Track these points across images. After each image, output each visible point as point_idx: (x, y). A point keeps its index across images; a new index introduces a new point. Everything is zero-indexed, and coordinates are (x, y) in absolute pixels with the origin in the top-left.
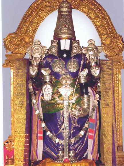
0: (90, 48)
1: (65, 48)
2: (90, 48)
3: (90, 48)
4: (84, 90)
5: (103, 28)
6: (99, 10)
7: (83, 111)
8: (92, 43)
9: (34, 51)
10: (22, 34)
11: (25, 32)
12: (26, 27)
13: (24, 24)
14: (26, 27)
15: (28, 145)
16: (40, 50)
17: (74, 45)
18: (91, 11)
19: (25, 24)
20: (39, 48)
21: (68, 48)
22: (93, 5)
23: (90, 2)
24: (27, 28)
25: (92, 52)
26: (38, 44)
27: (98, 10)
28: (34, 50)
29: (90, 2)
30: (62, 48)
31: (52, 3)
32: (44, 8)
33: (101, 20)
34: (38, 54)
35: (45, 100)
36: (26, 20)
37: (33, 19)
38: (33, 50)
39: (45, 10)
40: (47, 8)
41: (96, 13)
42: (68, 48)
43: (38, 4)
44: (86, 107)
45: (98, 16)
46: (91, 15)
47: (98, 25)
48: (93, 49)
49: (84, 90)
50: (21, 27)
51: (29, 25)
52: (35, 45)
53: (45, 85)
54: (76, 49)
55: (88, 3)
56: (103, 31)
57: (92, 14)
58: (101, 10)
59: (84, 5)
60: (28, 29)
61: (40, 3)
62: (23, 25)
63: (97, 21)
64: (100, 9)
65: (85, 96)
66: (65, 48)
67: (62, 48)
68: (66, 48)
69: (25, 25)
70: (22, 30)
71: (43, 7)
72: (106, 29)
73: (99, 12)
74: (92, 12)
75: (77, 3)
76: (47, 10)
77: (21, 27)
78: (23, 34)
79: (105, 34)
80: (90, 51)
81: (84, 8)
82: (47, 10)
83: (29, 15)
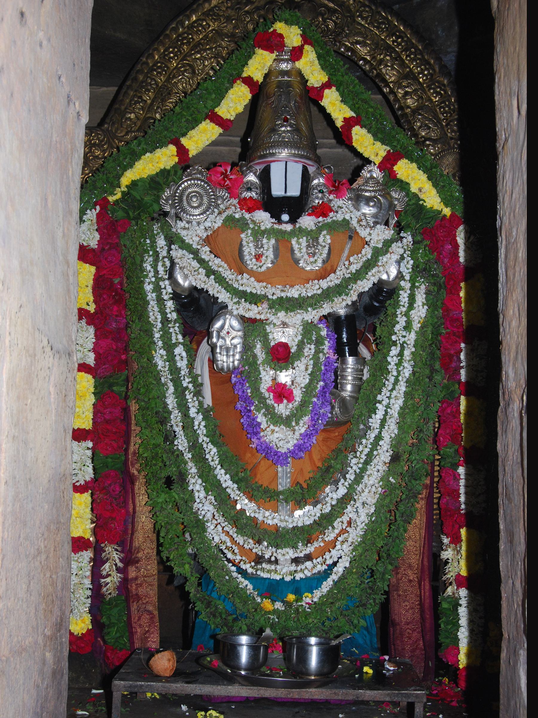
0: (367, 194)
1: (286, 192)
2: (367, 194)
3: (367, 191)
4: (344, 336)
5: (430, 120)
6: (415, 54)
7: (340, 408)
8: (375, 175)
9: (185, 203)
10: (127, 134)
11: (139, 123)
12: (143, 108)
13: (134, 96)
14: (143, 108)
15: (102, 691)
16: (205, 200)
17: (316, 182)
18: (385, 57)
19: (140, 97)
20: (201, 192)
21: (295, 191)
22: (390, 35)
23: (380, 23)
24: (148, 111)
25: (372, 206)
26: (198, 179)
27: (411, 53)
28: (185, 198)
29: (380, 23)
30: (277, 190)
31: (242, 21)
32: (213, 40)
33: (423, 89)
34: (197, 212)
35: (220, 366)
36: (142, 82)
37: (168, 80)
38: (181, 197)
39: (216, 48)
40: (223, 40)
41: (402, 64)
42: (295, 191)
43: (191, 26)
44: (349, 394)
45: (411, 76)
46: (384, 71)
47: (408, 107)
48: (375, 197)
49: (344, 336)
50: (126, 109)
51: (153, 101)
52: (190, 180)
53: (220, 317)
54: (320, 195)
55: (374, 27)
56: (430, 128)
57: (387, 66)
58: (421, 53)
59: (359, 34)
60: (148, 115)
61: (195, 22)
62: (131, 101)
63: (406, 93)
64: (416, 48)
65: (350, 360)
66: (286, 192)
67: (277, 190)
68: (289, 194)
69: (137, 102)
70: (130, 119)
71: (206, 37)
72: (439, 121)
73: (412, 60)
74: (388, 58)
75: (331, 25)
76: (223, 48)
77: (123, 108)
78: (131, 132)
79: (435, 142)
80: (367, 204)
81: (358, 42)
82: (223, 48)
83: (155, 64)
